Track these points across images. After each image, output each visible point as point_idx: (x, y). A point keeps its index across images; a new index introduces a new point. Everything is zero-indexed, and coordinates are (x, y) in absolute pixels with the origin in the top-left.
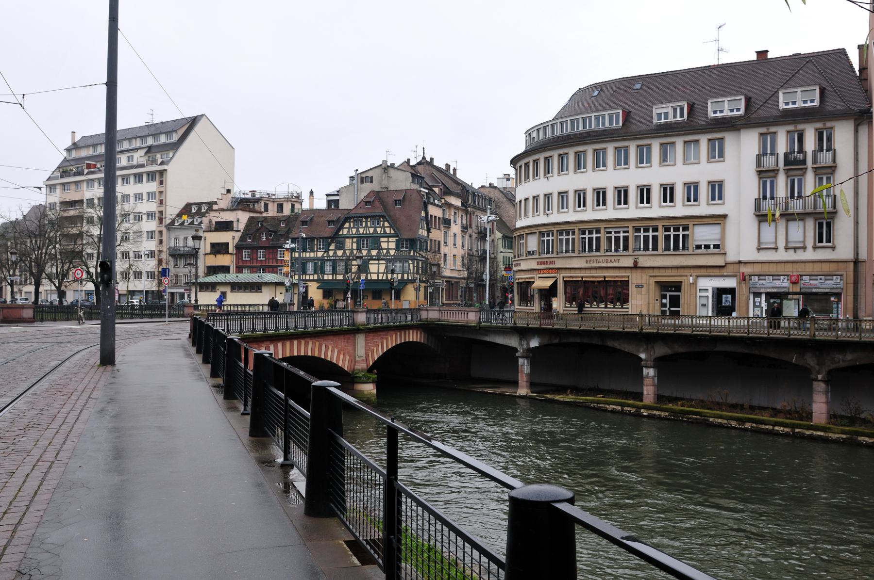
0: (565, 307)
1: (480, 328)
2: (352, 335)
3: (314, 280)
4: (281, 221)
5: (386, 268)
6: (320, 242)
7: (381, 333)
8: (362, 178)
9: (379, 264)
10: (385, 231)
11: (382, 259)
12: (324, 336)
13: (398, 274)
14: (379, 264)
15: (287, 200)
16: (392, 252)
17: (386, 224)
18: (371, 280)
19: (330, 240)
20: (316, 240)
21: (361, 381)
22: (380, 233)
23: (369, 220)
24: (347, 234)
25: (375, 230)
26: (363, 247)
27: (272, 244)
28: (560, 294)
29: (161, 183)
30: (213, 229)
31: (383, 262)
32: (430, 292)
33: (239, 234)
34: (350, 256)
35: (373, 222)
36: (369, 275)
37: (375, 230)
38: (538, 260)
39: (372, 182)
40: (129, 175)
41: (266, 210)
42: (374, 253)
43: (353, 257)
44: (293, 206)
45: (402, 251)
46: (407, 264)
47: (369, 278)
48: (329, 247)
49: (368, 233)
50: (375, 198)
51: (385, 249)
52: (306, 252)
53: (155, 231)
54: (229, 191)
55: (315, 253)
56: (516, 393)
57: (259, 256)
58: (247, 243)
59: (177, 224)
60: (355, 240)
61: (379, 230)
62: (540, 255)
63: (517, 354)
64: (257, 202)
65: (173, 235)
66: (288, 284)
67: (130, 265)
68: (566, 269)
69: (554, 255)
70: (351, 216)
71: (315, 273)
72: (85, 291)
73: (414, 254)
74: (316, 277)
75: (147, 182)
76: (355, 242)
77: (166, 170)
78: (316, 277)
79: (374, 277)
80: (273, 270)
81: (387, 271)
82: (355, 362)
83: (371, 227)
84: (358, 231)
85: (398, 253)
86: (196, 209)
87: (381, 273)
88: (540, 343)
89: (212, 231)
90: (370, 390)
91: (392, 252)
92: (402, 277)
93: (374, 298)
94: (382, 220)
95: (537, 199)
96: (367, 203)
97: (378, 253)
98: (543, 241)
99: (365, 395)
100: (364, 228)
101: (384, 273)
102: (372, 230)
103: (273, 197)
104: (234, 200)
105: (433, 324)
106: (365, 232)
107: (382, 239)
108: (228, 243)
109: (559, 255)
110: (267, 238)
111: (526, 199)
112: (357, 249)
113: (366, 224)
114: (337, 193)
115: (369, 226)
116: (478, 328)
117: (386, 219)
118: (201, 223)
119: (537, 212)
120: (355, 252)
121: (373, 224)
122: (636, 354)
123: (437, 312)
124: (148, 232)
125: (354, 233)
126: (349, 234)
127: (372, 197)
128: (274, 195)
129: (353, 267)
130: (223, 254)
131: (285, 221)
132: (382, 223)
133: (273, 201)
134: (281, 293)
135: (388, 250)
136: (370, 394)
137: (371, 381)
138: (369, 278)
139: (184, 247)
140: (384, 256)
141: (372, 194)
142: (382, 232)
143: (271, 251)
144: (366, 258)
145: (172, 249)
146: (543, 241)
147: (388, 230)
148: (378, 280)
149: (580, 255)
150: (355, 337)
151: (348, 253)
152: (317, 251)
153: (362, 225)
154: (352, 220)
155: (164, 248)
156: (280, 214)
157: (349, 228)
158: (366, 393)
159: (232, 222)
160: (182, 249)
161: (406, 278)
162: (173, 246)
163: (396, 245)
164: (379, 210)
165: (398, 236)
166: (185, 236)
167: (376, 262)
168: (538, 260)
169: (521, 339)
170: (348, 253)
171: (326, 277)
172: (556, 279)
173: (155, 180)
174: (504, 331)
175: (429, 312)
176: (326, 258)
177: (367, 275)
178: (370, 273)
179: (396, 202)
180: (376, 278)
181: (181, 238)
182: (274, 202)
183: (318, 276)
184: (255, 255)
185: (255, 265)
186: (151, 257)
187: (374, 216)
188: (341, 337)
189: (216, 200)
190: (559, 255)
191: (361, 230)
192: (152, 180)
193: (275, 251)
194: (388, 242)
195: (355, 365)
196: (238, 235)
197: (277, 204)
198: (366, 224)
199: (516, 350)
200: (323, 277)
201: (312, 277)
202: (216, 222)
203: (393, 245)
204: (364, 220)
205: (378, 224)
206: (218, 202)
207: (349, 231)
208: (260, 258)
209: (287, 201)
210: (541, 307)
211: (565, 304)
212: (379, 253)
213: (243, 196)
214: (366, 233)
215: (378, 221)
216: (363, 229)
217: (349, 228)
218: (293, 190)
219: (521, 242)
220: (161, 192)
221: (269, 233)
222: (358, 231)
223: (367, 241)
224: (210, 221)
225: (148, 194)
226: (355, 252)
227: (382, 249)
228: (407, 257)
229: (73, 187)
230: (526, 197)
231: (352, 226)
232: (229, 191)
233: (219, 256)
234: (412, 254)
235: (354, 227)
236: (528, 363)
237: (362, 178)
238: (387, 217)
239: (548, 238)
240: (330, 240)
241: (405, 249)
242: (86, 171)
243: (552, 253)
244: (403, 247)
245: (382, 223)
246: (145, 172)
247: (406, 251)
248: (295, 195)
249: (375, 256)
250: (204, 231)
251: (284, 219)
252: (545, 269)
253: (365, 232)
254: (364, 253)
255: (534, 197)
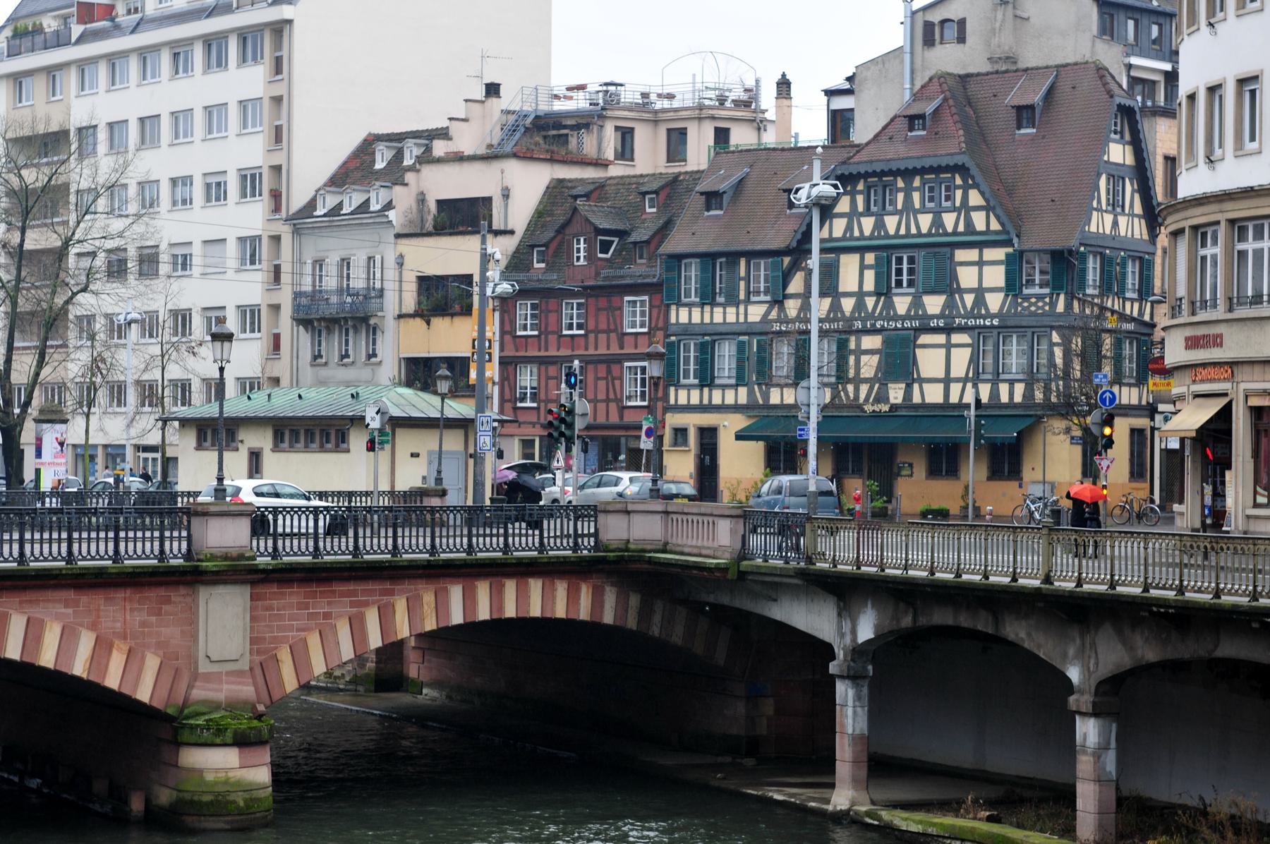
0: (1256, 505)
1: (742, 575)
2: (183, 590)
3: (736, 408)
4: (644, 194)
5: (974, 360)
6: (758, 268)
7: (351, 586)
8: (929, 26)
9: (949, 346)
10: (969, 223)
11: (962, 329)
12: (25, 588)
13: (1012, 383)
14: (949, 346)
15: (700, 113)
16: (994, 302)
17: (975, 198)
18: (924, 406)
19: (787, 260)
20: (743, 262)
21: (193, 739)
22: (955, 233)
23: (917, 182)
24: (843, 238)
25: (937, 223)
26: (899, 284)
27: (606, 278)
28: (1237, 455)
29: (278, 66)
30: (429, 226)
31: (963, 338)
32: (1167, 453)
33: (510, 244)
34: (852, 319)
35: (931, 190)
36: (916, 386)
37: (937, 223)
38: (1189, 332)
39: (961, 39)
40: (190, 41)
41: (625, 151)
42: (934, 304)
43: (864, 320)
44: (722, 136)
45: (1027, 298)
46: (1044, 347)
47: (917, 399)
48: (785, 286)
49: (914, 231)
50: (945, 100)
51: (970, 291)
52: (713, 304)
53: (260, 237)
54: (493, 90)
55: (742, 308)
56: (828, 802)
57: (565, 321)
58: (532, 274)
59: (320, 211)
60: (870, 258)
61: (949, 220)
62: (1231, 310)
63: (833, 668)
64: (587, 126)
65: (313, 247)
66: (375, 424)
67: (94, 360)
68: (1252, 363)
69: (1220, 313)
70: (854, 170)
71: (741, 380)
72: (105, 446)
73: (1069, 306)
74: (743, 395)
75: (239, 66)
76: (869, 267)
77: (290, 22)
78: (743, 395)
79: (934, 394)
80: (609, 371)
81: (977, 373)
82: (195, 676)
83: (924, 210)
84: (880, 225)
85: (1015, 304)
86: (389, 155)
87: (957, 380)
88: (877, 627)
89: (429, 234)
90: (227, 770)
91: (994, 302)
92: (1028, 394)
93: (934, 472)
94: (959, 181)
95: (1253, 92)
96: (913, 120)
97: (945, 306)
98: (1204, 258)
99: (207, 784)
100: (900, 213)
101: (965, 380)
102: (925, 221)
103: (666, 104)
104: (512, 118)
105: (640, 560)
106: (902, 231)
107: (960, 255)
108: (471, 276)
109: (1241, 312)
110: (590, 257)
111: (1214, 90)
112: (878, 294)
113: (908, 199)
114: (847, 86)
115: (917, 205)
116: (732, 575)
117: (973, 178)
118: (389, 206)
119: (1253, 139)
120: (870, 302)
121: (931, 199)
122: (1057, 663)
123: (658, 517)
124: (242, 240)
125: (867, 233)
126: (852, 238)
127: (931, 99)
128: (671, 97)
129: (864, 359)
130: (452, 315)
131: (656, 192)
132: (959, 193)
133: (655, 119)
134: (413, 455)
135: (980, 292)
136: (226, 782)
137: (229, 737)
138: (917, 399)
139: (340, 291)
140: (967, 317)
141: (935, 86)
142: (961, 228)
143: (603, 302)
144: (907, 324)
145: (304, 301)
146: (1204, 258)
147: (979, 220)
148: (946, 405)
149: (1236, 315)
150: (195, 595)
151: (848, 304)
152: (748, 301)
153: (893, 202)
154: (860, 187)
155: (285, 298)
156: (676, 169)
157: (853, 215)
158: (210, 777)
159: (488, 201)
160: (334, 299)
161: (1039, 396)
162: (308, 288)
163: (1008, 273)
164: (952, 147)
165: (1008, 243)
166: (344, 254)
167: (940, 339)
168: (1189, 332)
169: (839, 615)
170: (848, 304)
171: (775, 398)
172: (1224, 401)
173: (262, 58)
174: (776, 583)
175: (636, 519)
176: (776, 327)
177: (909, 387)
178: (922, 381)
179: (1024, 114)
180: (940, 400)
181: (332, 260)
182: (656, 122)
183: (751, 393)
184: (552, 318)
185: (552, 352)
186: (253, 331)
187: (932, 170)
188: (120, 594)
189: (445, 124)
190: (1241, 312)
191: (891, 222)
192: (255, 59)
193: (615, 299)
194: (980, 263)
195: (190, 687)
196: (501, 249)
197: (669, 130)
198: (908, 199)
199: (826, 651)
200: (766, 396)
201: (730, 398)
202: (439, 202)
203: (996, 276)
204: (900, 184)
205: (948, 198)
206: (455, 128)
207: (849, 228)
208: (570, 327)
209: (700, 119)
210: (1203, 507)
211: (1255, 493)
212: (949, 305)
213: (544, 107)
214: (908, 235)
215: (948, 189)
216: (896, 218)
217: (853, 215)
218: (734, 80)
219: (1208, 251)
220: (278, 100)
221: (600, 237)
222: (880, 225)
223: (911, 260)
224: (421, 199)
225: (243, 104)
226: (870, 302)
227: (961, 291)
228: (1047, 321)
229: (39, 86)
230: (1213, 80)
231: (861, 208)
232: (493, 90)
233: (441, 324)
234: (1060, 307)
235: (868, 212)
236: (858, 697)
237: (929, 26)
238: (974, 171)
239: (1258, 245)
240: (787, 260)
241: (1037, 290)
242: (77, 30)
243: (1215, 306)
244: (1030, 283)
245: (959, 193)
246: (232, 31)
247: (1040, 297)
248: (737, 93)
249: (937, 317)
250: (398, 236)
251: (655, 186)
252: (1204, 365)
253: (902, 231)
254: (902, 304)
255: (1241, 82)
